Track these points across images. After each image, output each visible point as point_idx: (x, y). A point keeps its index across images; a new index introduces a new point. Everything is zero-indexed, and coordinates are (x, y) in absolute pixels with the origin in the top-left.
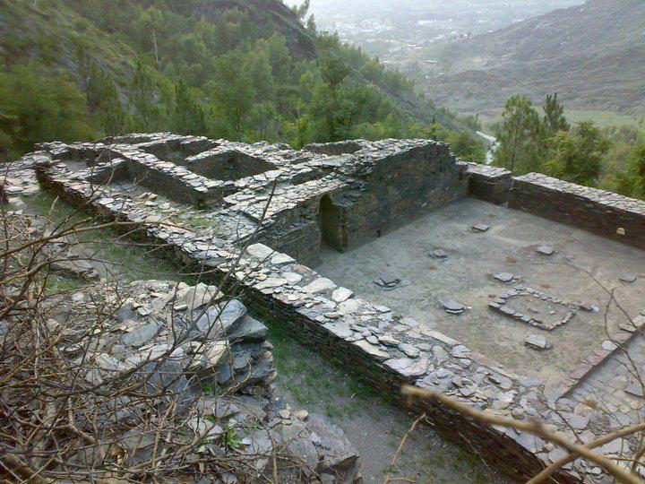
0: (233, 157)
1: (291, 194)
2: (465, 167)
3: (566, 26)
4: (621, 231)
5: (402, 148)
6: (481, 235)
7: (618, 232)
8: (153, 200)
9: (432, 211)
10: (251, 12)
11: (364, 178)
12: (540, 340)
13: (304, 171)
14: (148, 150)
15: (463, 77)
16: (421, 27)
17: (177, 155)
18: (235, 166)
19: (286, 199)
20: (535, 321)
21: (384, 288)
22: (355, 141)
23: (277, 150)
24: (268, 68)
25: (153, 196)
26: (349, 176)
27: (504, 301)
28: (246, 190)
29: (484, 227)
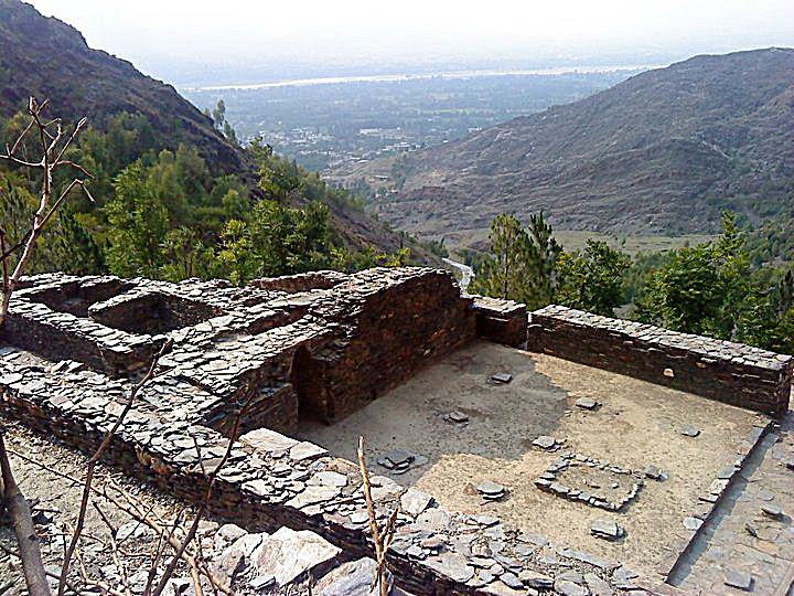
0: (157, 300)
1: (252, 348)
2: (471, 301)
3: (529, 136)
4: (669, 372)
5: (397, 279)
6: (505, 387)
7: (665, 374)
8: (76, 371)
9: (437, 360)
10: (152, 118)
11: (350, 320)
12: (609, 524)
13: (264, 315)
14: (34, 298)
15: (420, 195)
16: (364, 137)
17: (76, 302)
18: (156, 314)
19: (245, 355)
20: (597, 499)
21: (394, 471)
22: (320, 272)
23: (214, 289)
24: (179, 189)
25: (75, 365)
26: (330, 319)
27: (552, 476)
28: (186, 346)
29: (506, 377)
